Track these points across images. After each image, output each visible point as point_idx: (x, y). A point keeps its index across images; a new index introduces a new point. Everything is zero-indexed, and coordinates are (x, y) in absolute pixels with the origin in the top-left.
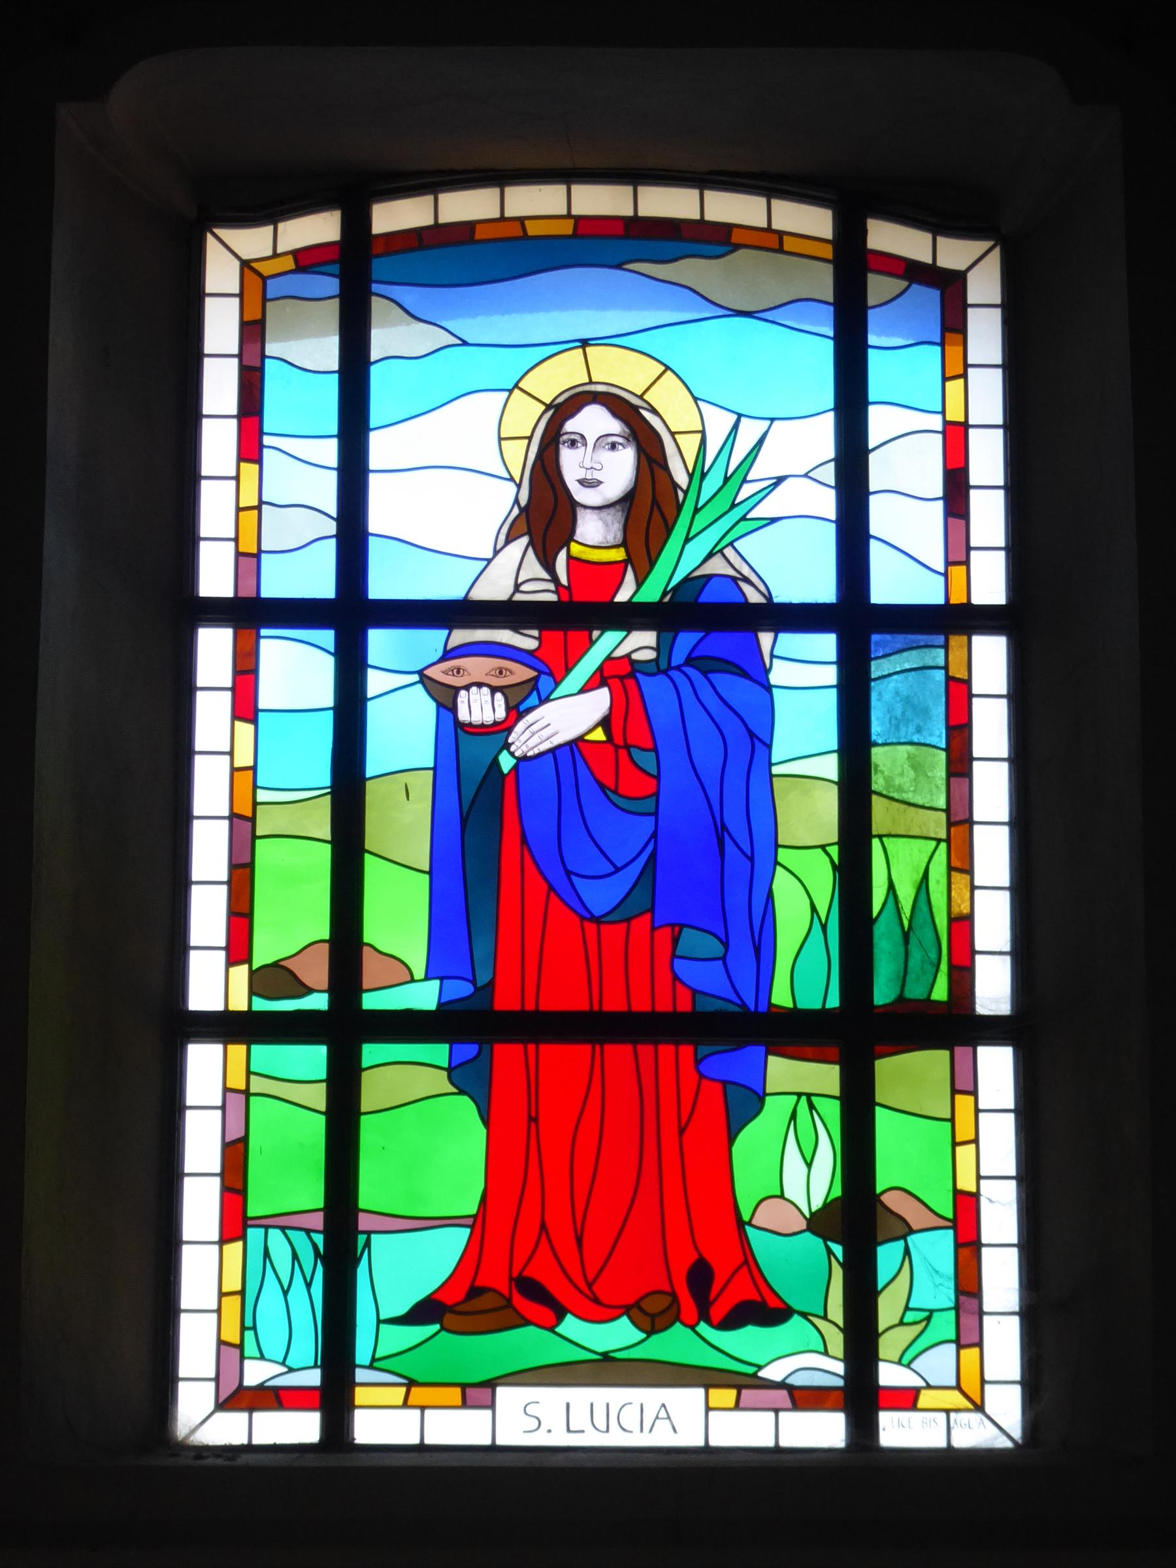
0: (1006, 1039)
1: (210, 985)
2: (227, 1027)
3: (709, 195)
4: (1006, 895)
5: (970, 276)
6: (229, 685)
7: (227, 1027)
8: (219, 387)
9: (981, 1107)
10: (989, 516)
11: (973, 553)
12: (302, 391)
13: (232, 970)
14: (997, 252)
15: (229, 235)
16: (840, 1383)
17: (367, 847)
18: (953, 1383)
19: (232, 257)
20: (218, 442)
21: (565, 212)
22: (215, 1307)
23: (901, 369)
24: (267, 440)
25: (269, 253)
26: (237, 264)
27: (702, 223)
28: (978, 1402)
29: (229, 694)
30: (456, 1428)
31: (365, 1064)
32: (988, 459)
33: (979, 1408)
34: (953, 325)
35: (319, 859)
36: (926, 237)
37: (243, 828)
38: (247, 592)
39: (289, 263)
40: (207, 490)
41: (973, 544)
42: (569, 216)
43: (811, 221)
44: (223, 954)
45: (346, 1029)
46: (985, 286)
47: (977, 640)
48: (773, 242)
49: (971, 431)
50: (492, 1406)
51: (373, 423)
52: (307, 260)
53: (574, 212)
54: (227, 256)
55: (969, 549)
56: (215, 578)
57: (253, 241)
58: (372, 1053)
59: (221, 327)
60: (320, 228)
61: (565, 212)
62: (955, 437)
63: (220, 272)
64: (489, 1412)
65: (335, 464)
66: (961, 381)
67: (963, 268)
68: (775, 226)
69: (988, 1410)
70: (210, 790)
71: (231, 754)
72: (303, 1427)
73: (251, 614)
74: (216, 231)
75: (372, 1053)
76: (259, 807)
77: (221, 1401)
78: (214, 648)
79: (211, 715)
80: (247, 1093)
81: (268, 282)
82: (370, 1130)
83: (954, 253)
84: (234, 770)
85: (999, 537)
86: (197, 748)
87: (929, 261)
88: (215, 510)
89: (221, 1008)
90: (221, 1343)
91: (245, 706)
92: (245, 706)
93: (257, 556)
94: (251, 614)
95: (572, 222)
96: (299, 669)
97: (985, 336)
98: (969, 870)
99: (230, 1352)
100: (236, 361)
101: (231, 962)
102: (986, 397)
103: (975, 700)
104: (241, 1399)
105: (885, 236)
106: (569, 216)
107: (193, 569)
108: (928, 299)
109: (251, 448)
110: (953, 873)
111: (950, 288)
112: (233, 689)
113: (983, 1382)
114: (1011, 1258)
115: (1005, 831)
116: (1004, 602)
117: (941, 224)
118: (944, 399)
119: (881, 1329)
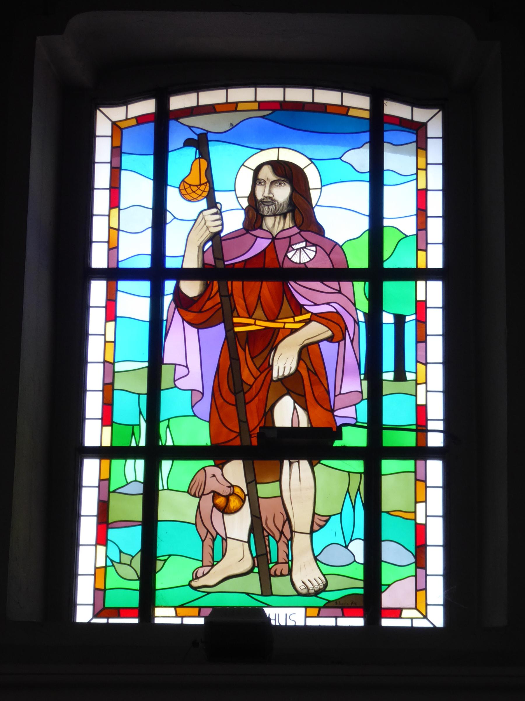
0: (439, 457)
1: (94, 434)
2: (103, 453)
3: (317, 91)
4: (441, 366)
5: (429, 124)
6: (104, 305)
7: (103, 453)
8: (102, 176)
9: (428, 162)
10: (436, 230)
11: (429, 246)
12: (138, 188)
13: (108, 324)
14: (441, 113)
15: (108, 111)
18: (414, 607)
19: (108, 120)
20: (101, 200)
21: (254, 100)
22: (107, 214)
23: (398, 161)
25: (125, 118)
26: (110, 123)
28: (425, 614)
29: (104, 309)
32: (435, 204)
34: (422, 146)
36: (409, 108)
37: (108, 390)
38: (113, 265)
39: (134, 122)
40: (96, 220)
41: (428, 242)
42: (255, 101)
43: (359, 103)
44: (100, 421)
45: (154, 453)
46: (435, 129)
47: (429, 462)
48: (343, 111)
49: (428, 192)
52: (141, 120)
53: (258, 99)
54: (104, 121)
55: (427, 244)
56: (99, 259)
57: (117, 113)
59: (103, 150)
61: (254, 100)
62: (422, 195)
63: (103, 126)
65: (151, 207)
67: (425, 121)
68: (344, 104)
69: (428, 617)
70: (95, 350)
71: (105, 335)
73: (114, 274)
74: (101, 109)
76: (116, 374)
77: (95, 614)
78: (98, 290)
79: (96, 318)
80: (118, 230)
81: (124, 131)
83: (421, 115)
84: (106, 342)
85: (440, 330)
86: (94, 213)
87: (410, 118)
88: (99, 230)
89: (99, 445)
90: (110, 228)
91: (111, 314)
92: (111, 314)
93: (104, 590)
94: (114, 274)
95: (257, 104)
96: (134, 300)
97: (435, 150)
98: (425, 568)
99: (100, 592)
100: (109, 165)
101: (104, 424)
102: (435, 178)
103: (428, 309)
105: (393, 109)
106: (255, 101)
107: (82, 432)
109: (115, 202)
110: (417, 482)
111: (419, 130)
112: (106, 307)
113: (427, 605)
114: (440, 340)
115: (441, 549)
116: (441, 445)
117: (415, 102)
118: (416, 179)
119: (384, 259)
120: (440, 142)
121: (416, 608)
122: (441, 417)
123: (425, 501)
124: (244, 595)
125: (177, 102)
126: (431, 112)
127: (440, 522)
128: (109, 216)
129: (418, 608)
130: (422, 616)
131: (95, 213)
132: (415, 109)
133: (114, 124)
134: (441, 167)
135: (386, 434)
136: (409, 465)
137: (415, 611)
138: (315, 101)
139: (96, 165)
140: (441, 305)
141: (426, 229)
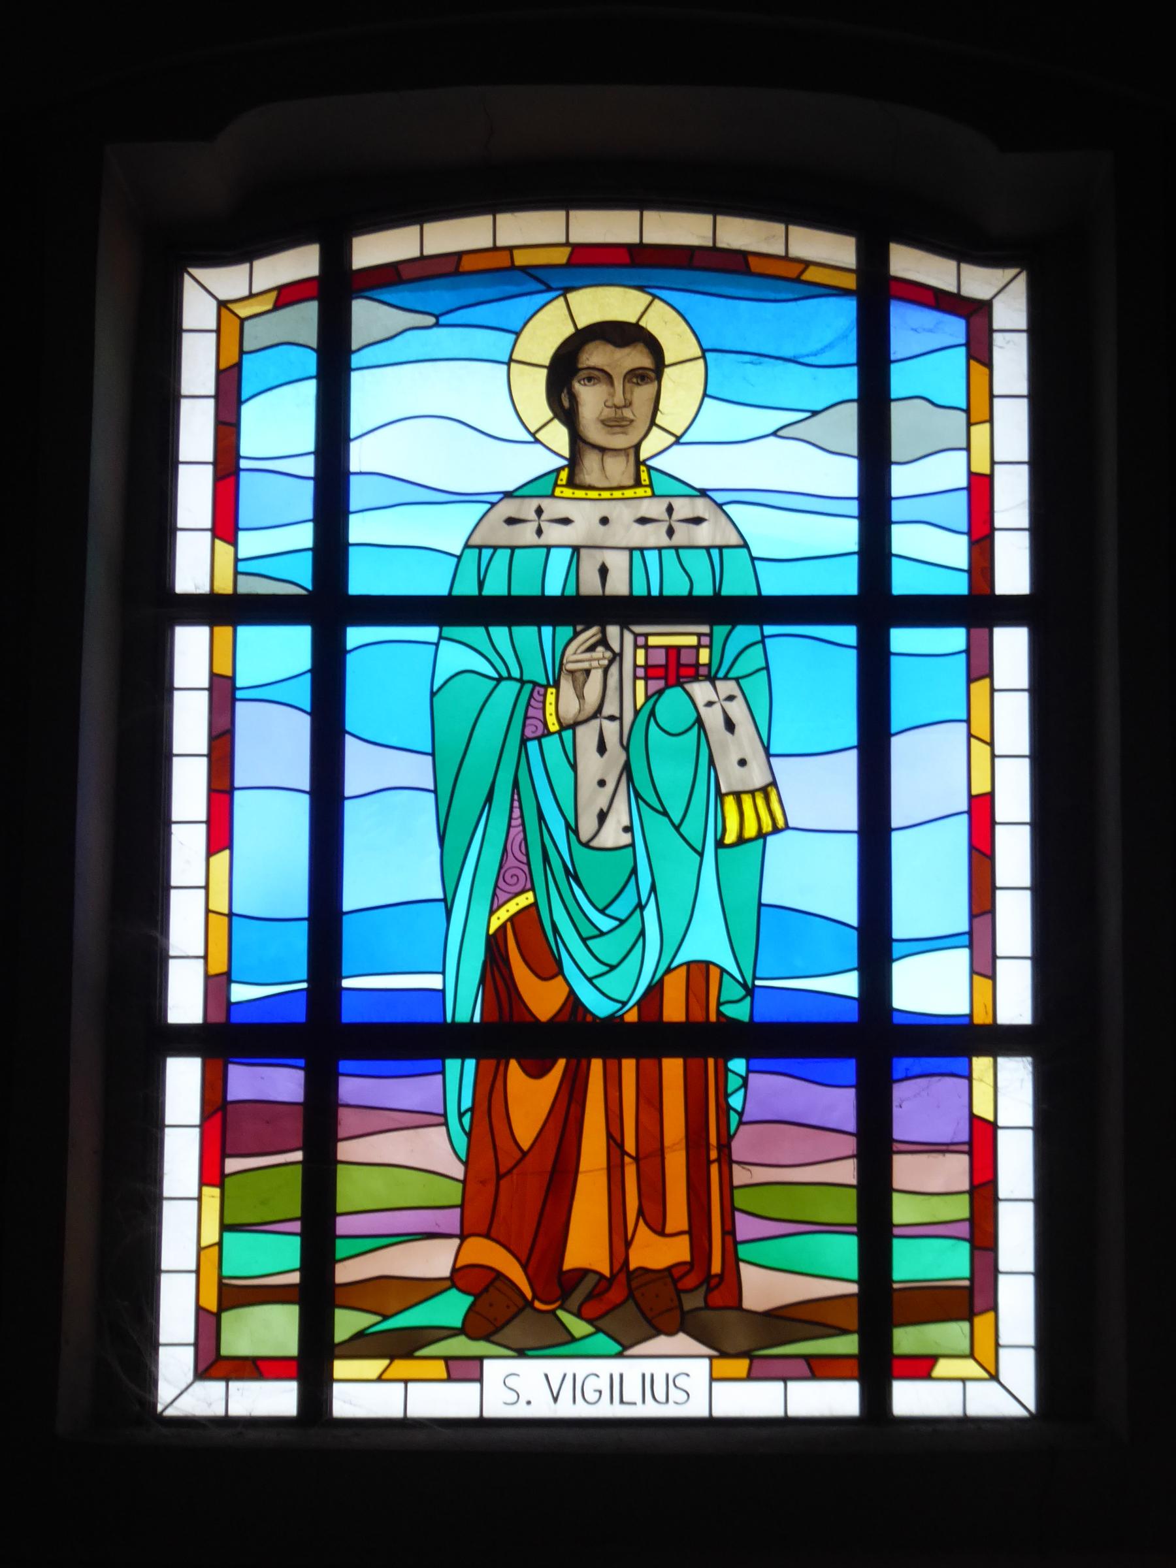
4: (1028, 893)
15: (204, 274)
16: (853, 1288)
17: (348, 727)
18: (967, 1351)
21: (563, 240)
24: (244, 464)
26: (214, 303)
27: (714, 250)
28: (993, 1372)
29: (205, 760)
30: (439, 1400)
31: (349, 646)
33: (994, 1377)
35: (297, 812)
46: (1011, 312)
50: (480, 1380)
51: (353, 506)
52: (287, 296)
53: (572, 240)
54: (202, 296)
57: (229, 281)
58: (355, 635)
60: (301, 263)
63: (197, 310)
64: (477, 1386)
66: (987, 425)
72: (278, 1399)
75: (355, 635)
82: (354, 815)
83: (978, 282)
85: (1024, 877)
103: (998, 893)
104: (213, 1364)
105: (907, 263)
108: (955, 328)
111: (976, 315)
114: (1024, 900)
115: (1026, 762)
120: (1022, 340)
121: (972, 1355)
122: (1026, 751)
123: (991, 421)
124: (631, 864)
125: (371, 250)
126: (1000, 275)
127: (1022, 475)
128: (199, 1199)
129: (976, 1355)
130: (986, 1375)
131: (164, 1267)
132: (964, 266)
133: (223, 305)
134: (1024, 403)
135: (900, 1247)
136: (954, 638)
137: (971, 1362)
138: (686, 1227)
139: (175, 759)
140: (1025, 685)
141: (992, 911)
